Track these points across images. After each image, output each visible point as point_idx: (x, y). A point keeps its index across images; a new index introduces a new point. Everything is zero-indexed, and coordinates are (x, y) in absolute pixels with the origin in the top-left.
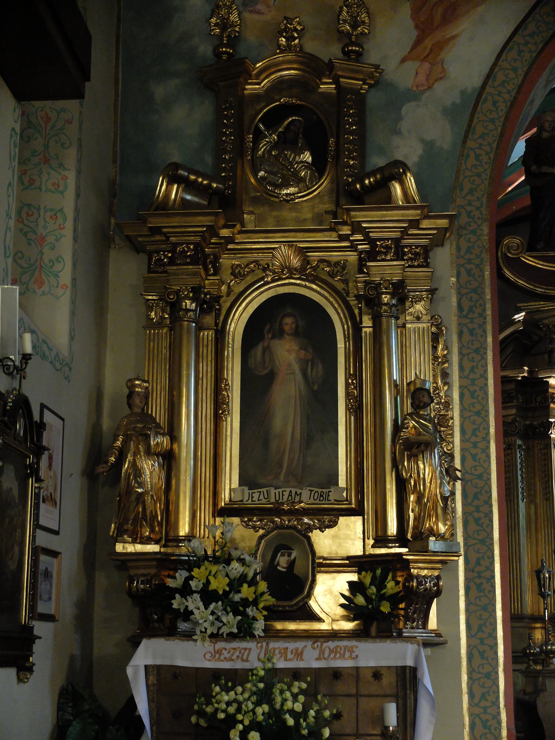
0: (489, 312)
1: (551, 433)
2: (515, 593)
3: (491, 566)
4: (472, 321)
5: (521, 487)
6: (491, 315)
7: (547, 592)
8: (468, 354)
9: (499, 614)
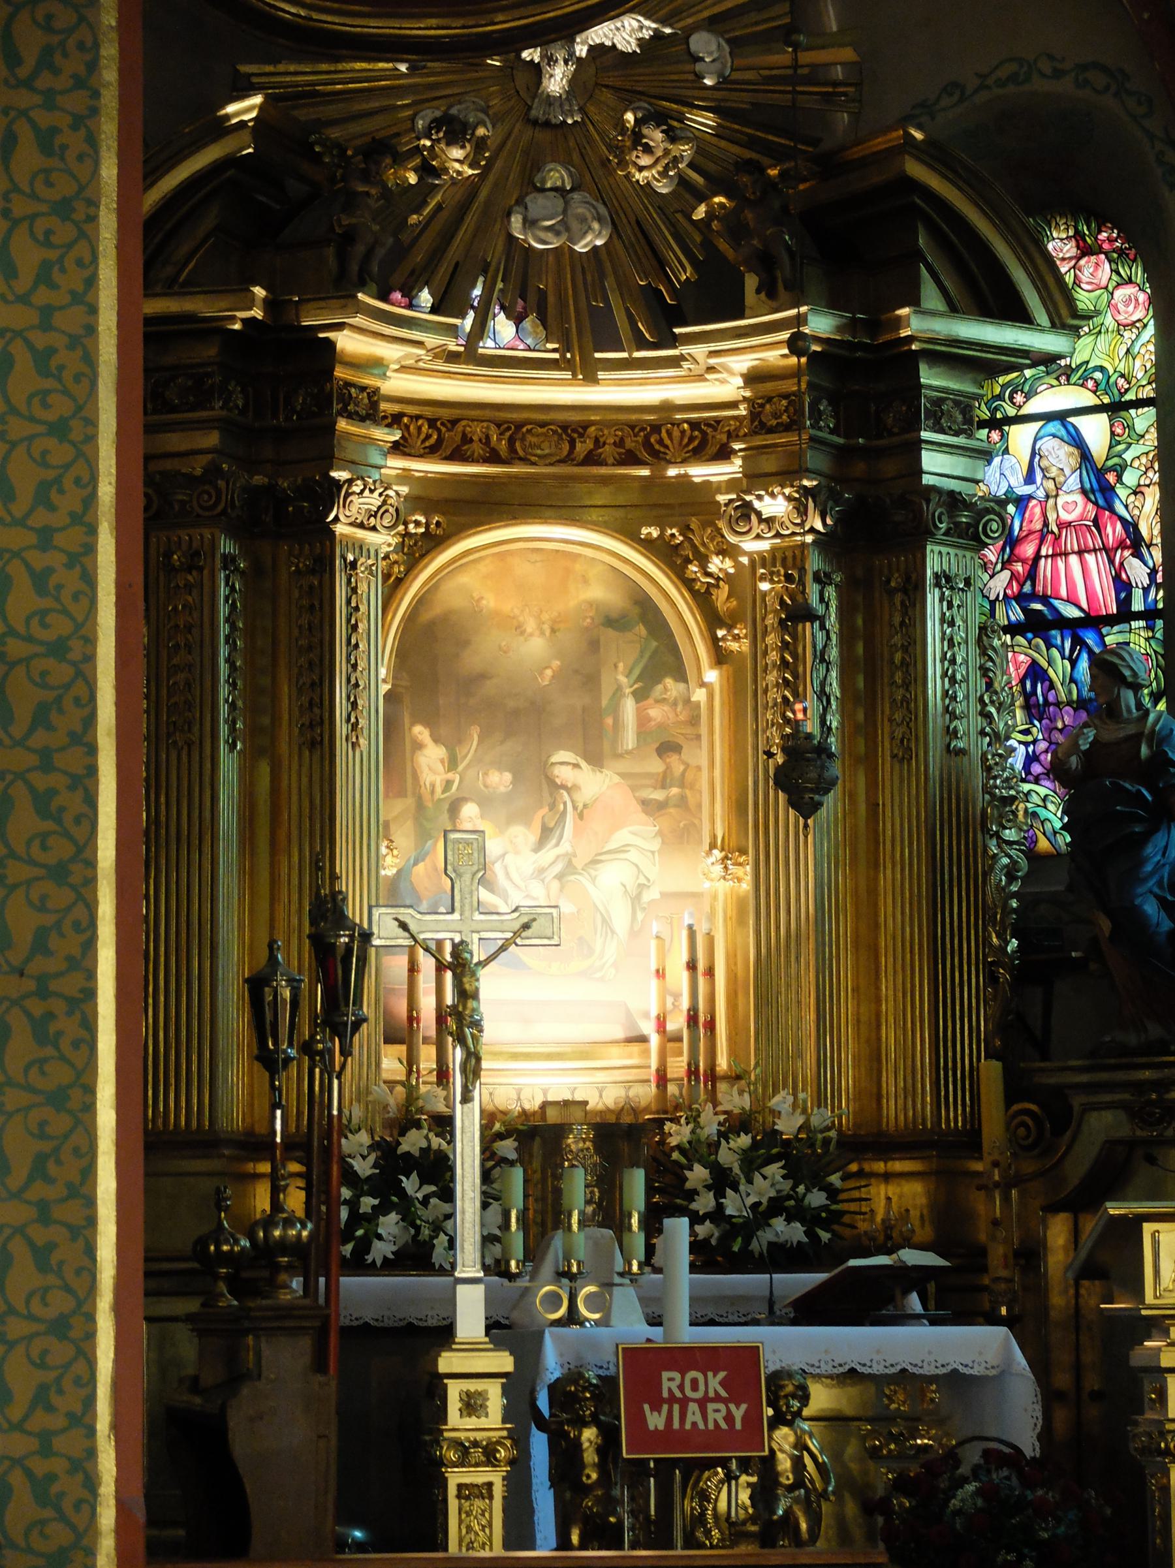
0: (110, 75)
1: (337, 519)
2: (195, 1058)
3: (84, 954)
4: (50, 100)
5: (226, 701)
6: (115, 84)
7: (285, 1052)
8: (33, 217)
9: (106, 1118)
